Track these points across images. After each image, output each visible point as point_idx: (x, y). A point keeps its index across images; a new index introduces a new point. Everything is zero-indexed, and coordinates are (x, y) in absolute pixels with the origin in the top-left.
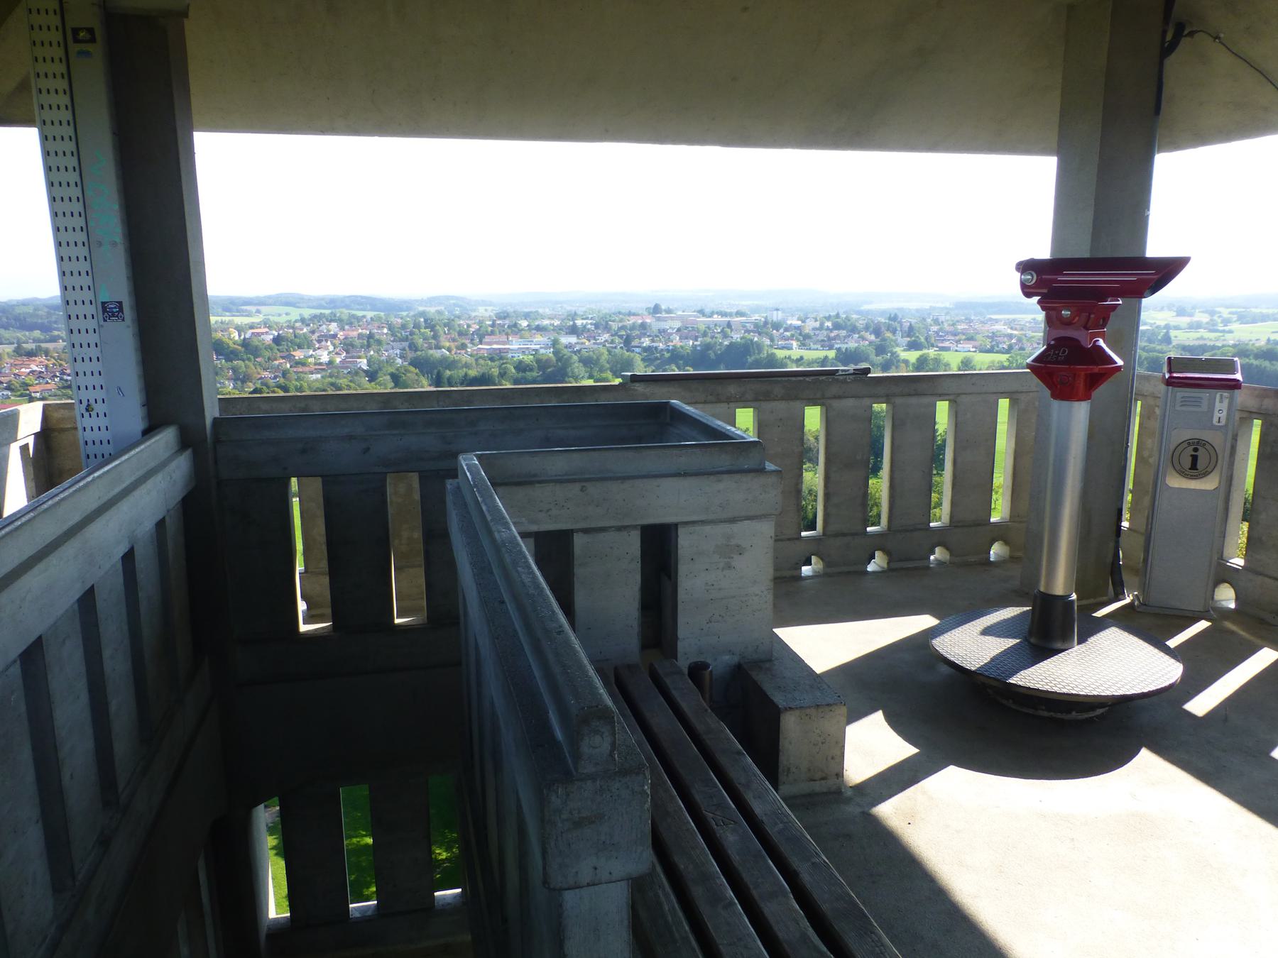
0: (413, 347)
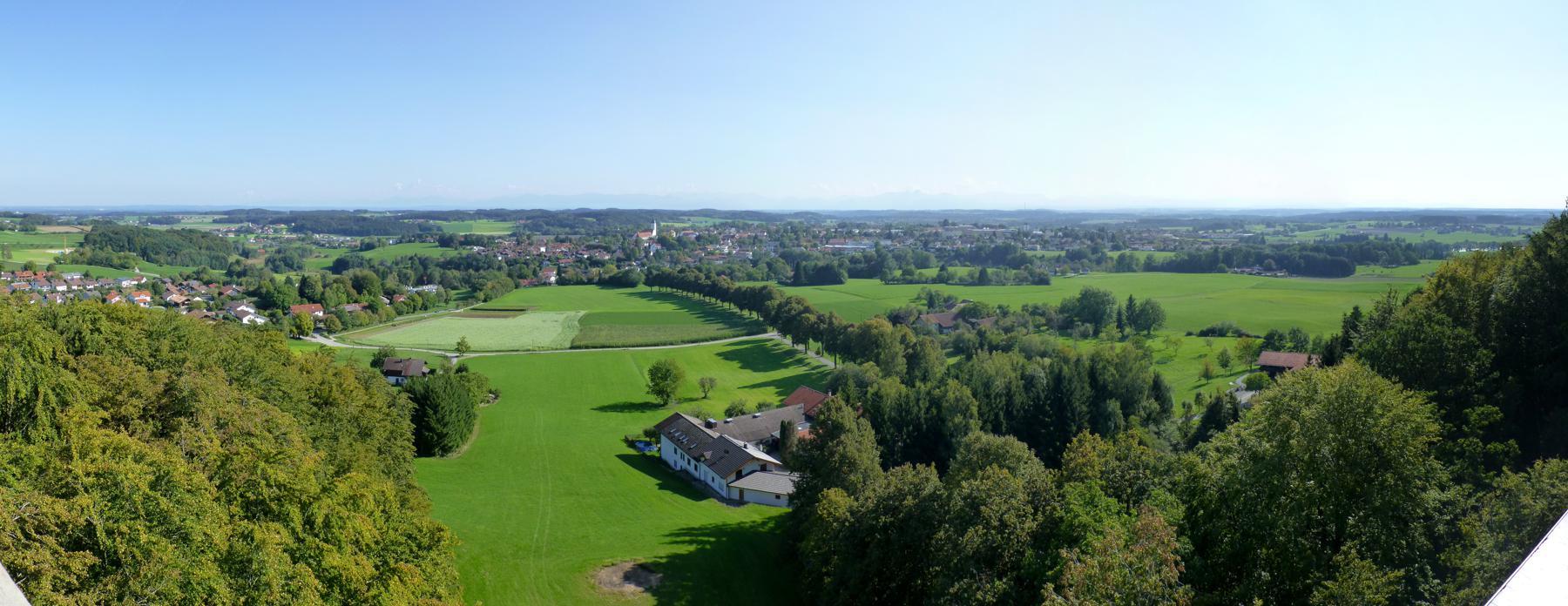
0: (783, 245)
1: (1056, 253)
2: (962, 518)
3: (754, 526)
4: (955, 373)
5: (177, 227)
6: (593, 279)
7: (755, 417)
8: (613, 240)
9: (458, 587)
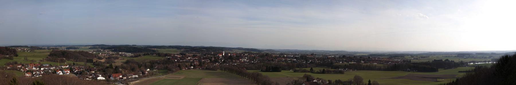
5: (78, 50)
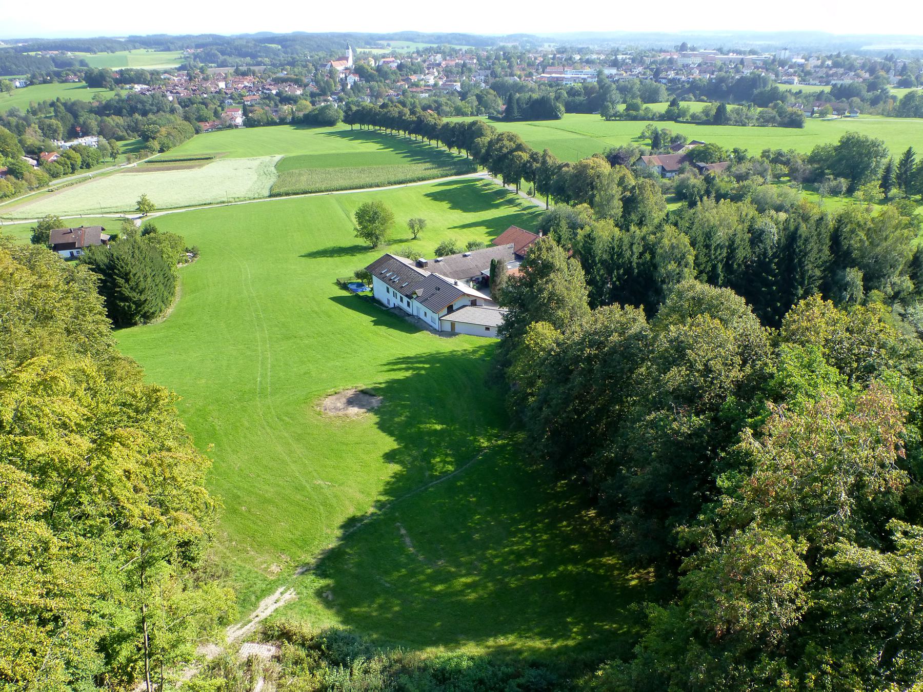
0: (494, 75)
1: (818, 89)
2: (665, 358)
3: (465, 353)
4: (675, 220)
6: (285, 118)
7: (465, 256)
8: (304, 71)
9: (187, 437)
